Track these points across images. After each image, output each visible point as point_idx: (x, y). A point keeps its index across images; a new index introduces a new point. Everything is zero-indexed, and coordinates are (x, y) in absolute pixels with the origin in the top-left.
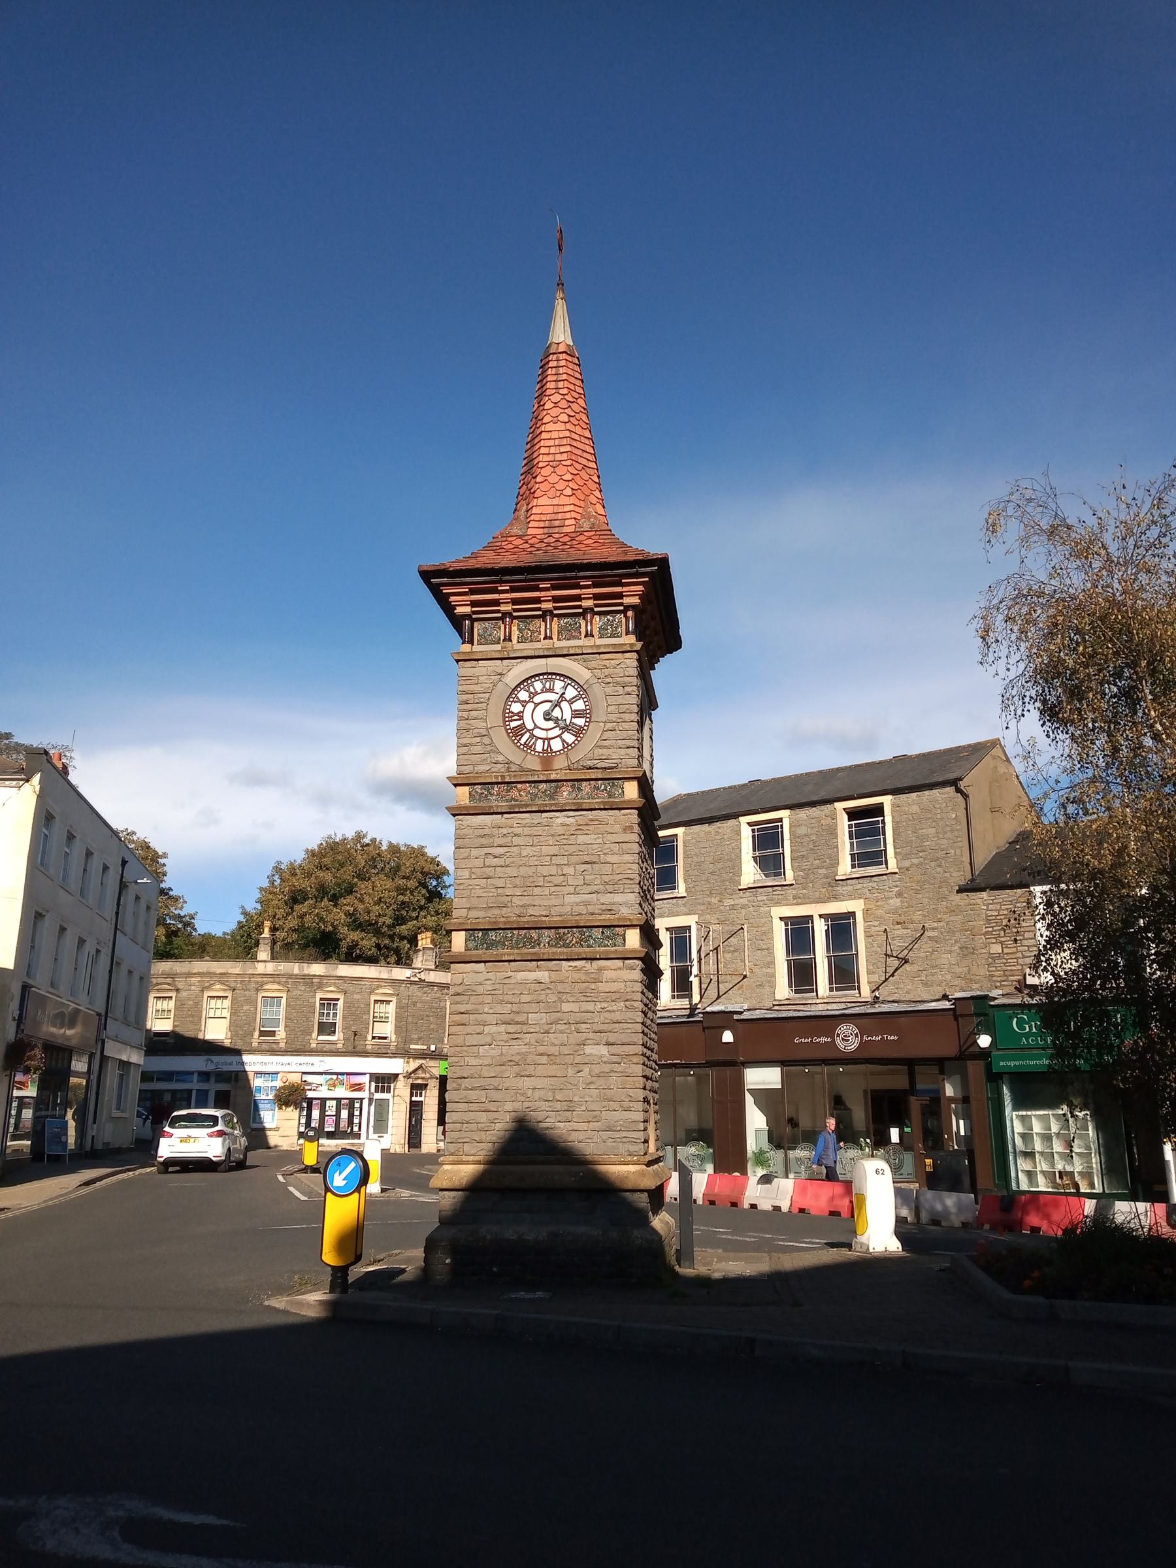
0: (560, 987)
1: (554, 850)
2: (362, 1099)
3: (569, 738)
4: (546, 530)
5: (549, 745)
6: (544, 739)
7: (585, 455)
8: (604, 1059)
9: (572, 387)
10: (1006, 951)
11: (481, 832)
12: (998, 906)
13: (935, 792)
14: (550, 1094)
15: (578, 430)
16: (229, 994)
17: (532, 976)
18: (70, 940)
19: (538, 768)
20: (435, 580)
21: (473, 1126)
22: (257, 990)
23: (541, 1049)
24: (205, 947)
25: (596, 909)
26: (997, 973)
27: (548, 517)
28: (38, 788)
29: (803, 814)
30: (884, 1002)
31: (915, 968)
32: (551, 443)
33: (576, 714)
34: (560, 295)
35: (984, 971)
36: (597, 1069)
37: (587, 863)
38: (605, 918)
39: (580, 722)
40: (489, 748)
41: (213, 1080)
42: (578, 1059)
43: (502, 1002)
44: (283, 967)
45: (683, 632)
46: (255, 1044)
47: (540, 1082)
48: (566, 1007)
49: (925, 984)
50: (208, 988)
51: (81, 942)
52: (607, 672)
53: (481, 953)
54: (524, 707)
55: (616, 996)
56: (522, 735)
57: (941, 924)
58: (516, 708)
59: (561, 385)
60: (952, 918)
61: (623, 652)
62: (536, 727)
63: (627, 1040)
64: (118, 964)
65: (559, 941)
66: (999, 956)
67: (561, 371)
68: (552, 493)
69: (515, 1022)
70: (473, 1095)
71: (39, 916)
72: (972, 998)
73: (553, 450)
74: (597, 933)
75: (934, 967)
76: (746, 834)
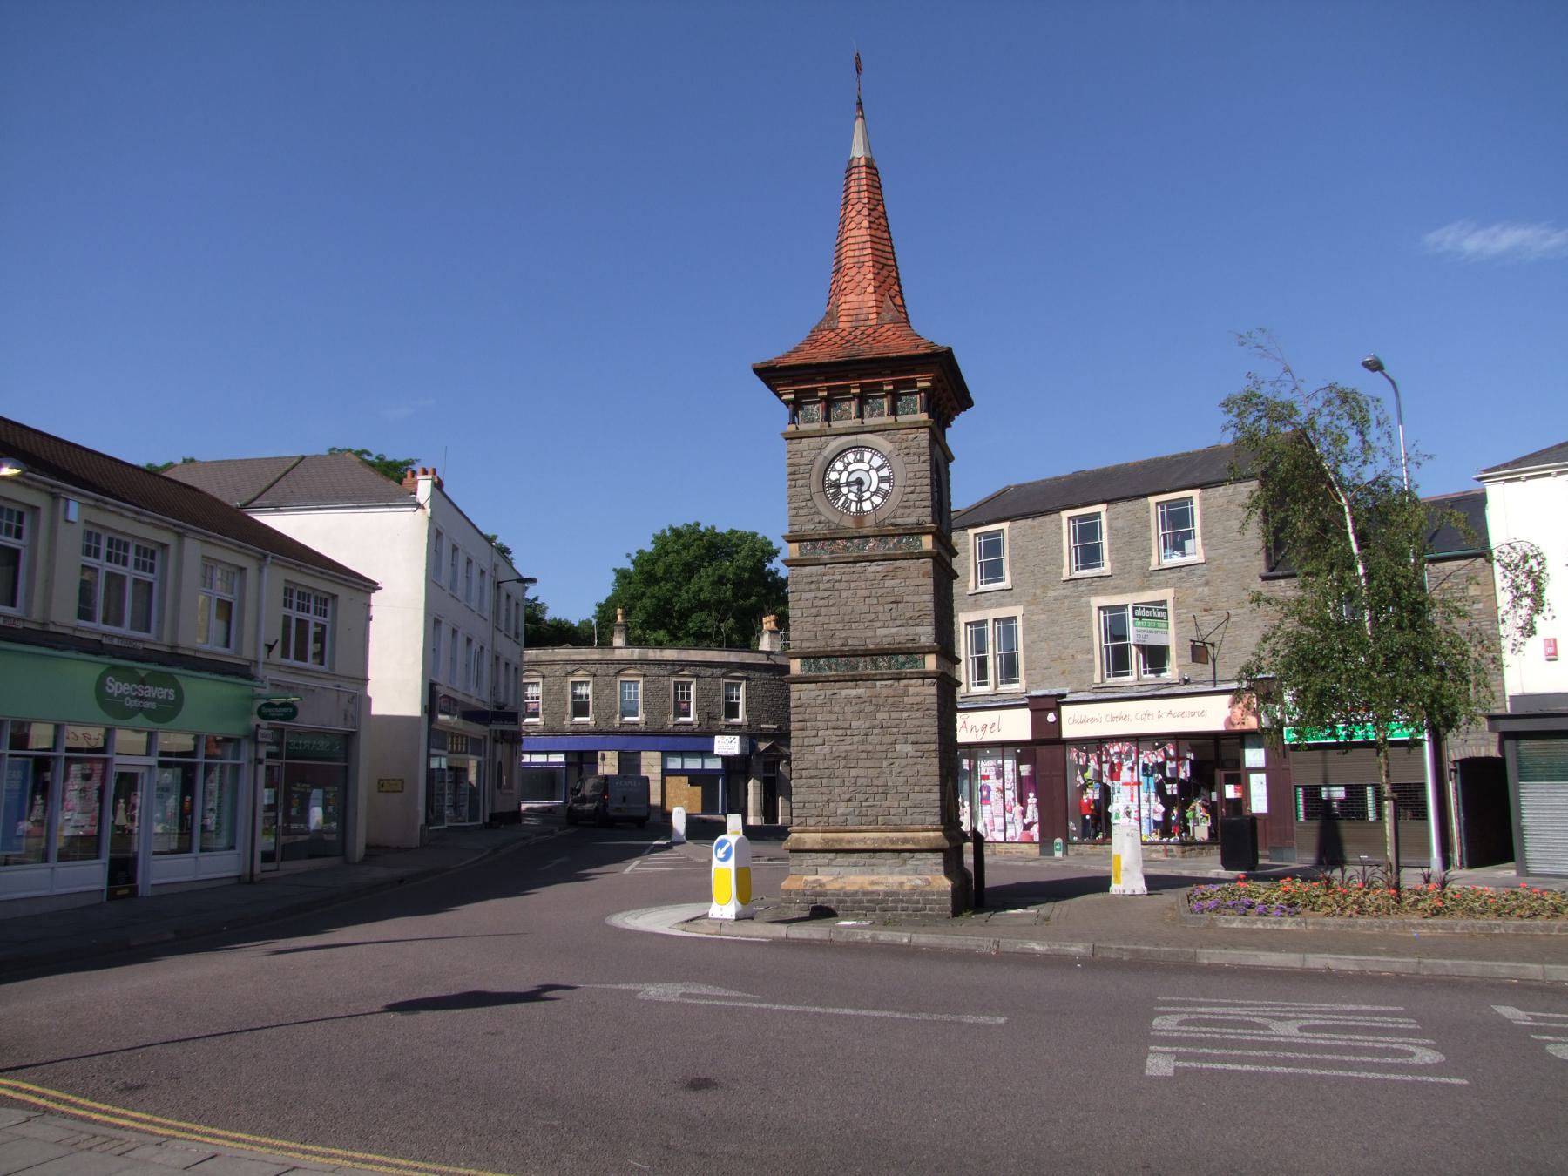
1: (867, 593)
17: (854, 692)
20: (770, 375)
24: (562, 635)
25: (902, 639)
29: (1121, 507)
33: (882, 480)
34: (859, 123)
36: (903, 762)
44: (636, 653)
45: (972, 395)
48: (879, 716)
50: (572, 674)
55: (917, 706)
69: (845, 732)
71: (437, 622)
76: (1065, 521)
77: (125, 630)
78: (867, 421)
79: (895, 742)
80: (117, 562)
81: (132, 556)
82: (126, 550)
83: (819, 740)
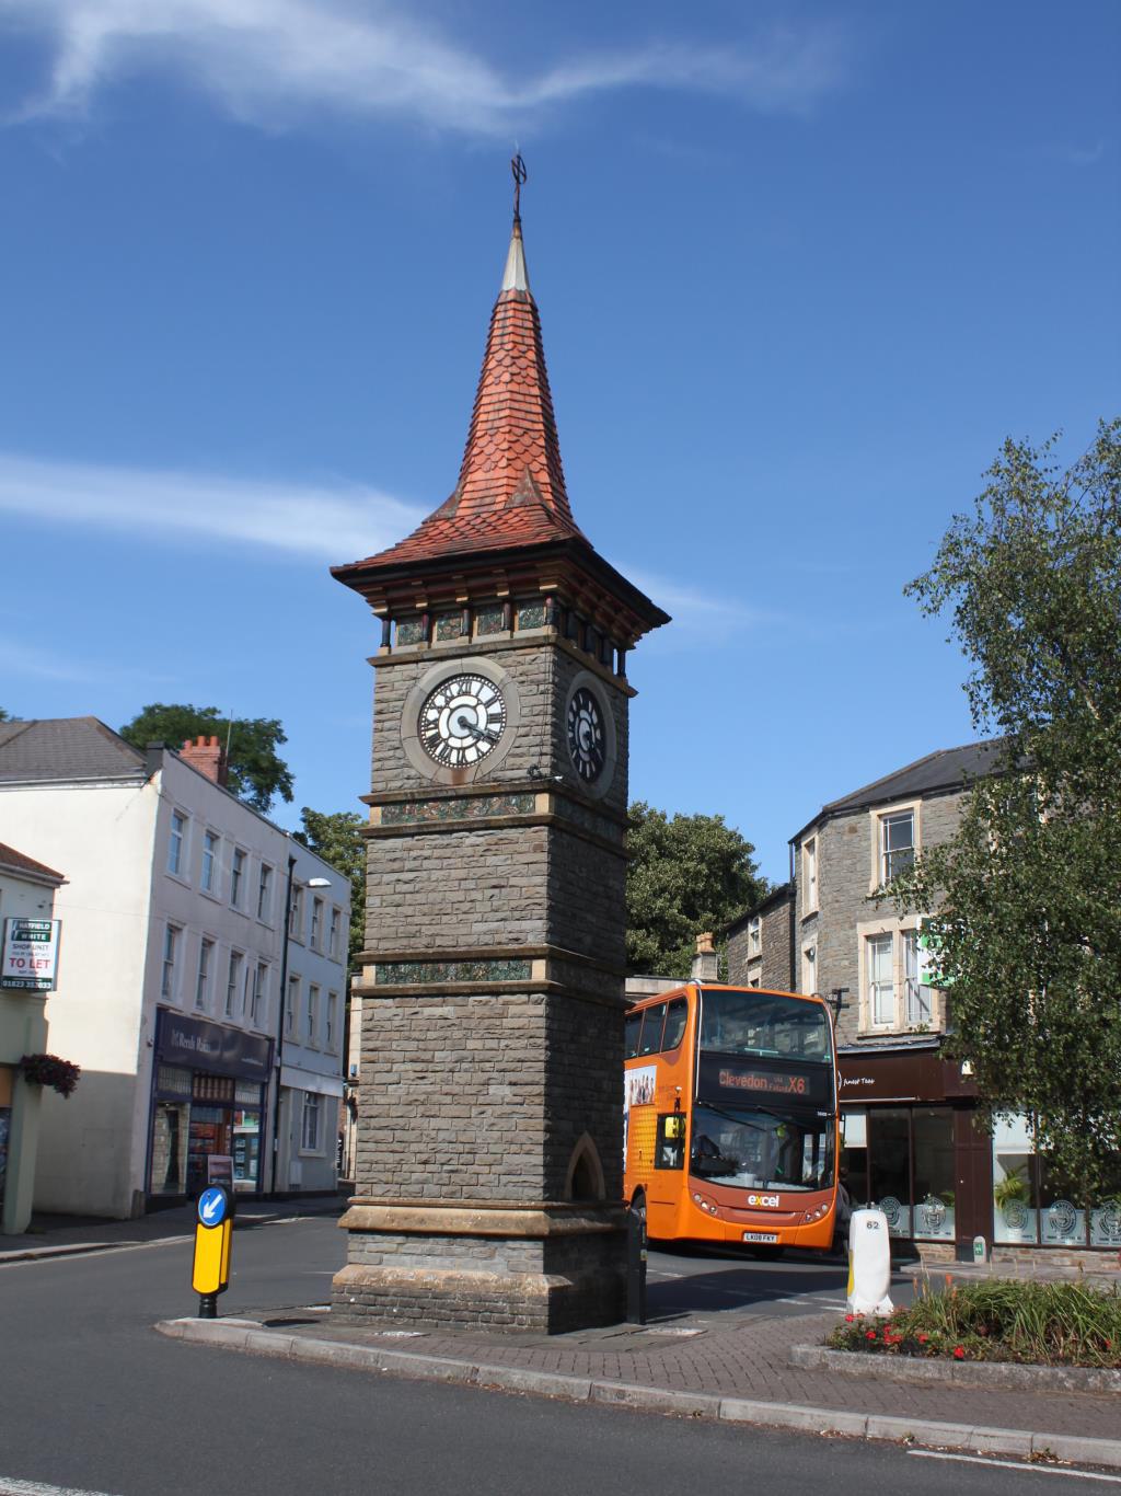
0: (465, 1023)
1: (462, 873)
3: (484, 746)
4: (476, 510)
5: (464, 756)
6: (458, 749)
8: (506, 1100)
9: (519, 339)
11: (393, 856)
14: (454, 1135)
15: (523, 389)
17: (438, 1011)
18: (218, 958)
19: (449, 782)
21: (381, 1167)
23: (446, 1089)
25: (503, 938)
27: (480, 494)
28: (159, 787)
32: (490, 408)
33: (492, 719)
36: (498, 1110)
37: (494, 887)
39: (495, 727)
40: (402, 762)
42: (481, 1099)
43: (408, 1039)
48: (471, 1044)
51: (236, 956)
52: (521, 669)
54: (440, 713)
55: (519, 1032)
56: (437, 746)
58: (432, 715)
59: (506, 339)
61: (514, 649)
62: (451, 735)
64: (293, 980)
67: (508, 322)
68: (486, 467)
70: (381, 1134)
71: (173, 930)
73: (491, 416)
74: (503, 965)
79: (486, 1084)
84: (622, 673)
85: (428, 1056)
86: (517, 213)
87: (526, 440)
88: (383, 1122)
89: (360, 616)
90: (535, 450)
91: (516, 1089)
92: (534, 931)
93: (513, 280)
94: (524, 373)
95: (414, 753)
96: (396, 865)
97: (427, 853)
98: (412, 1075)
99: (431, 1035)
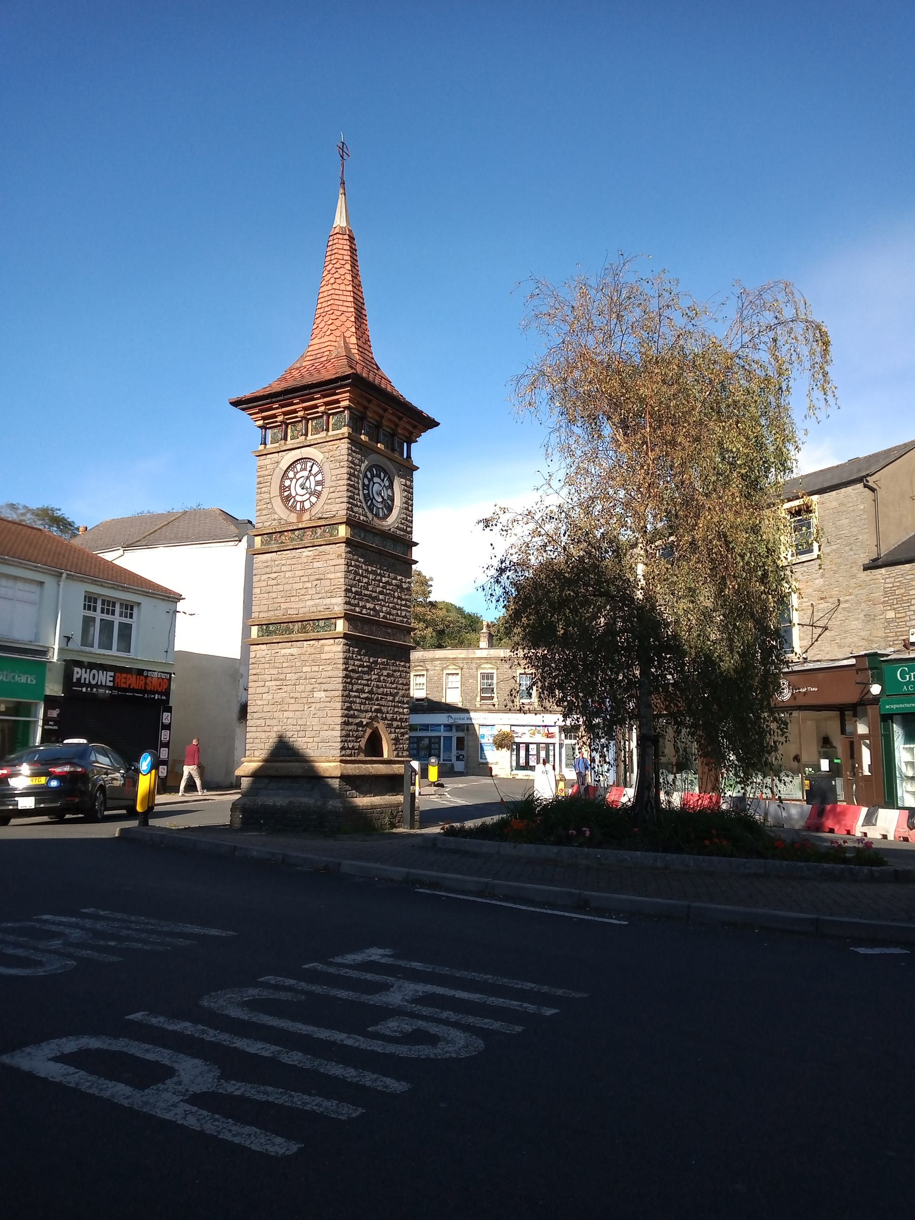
2: (554, 744)
3: (313, 499)
7: (345, 304)
10: (898, 616)
12: (892, 580)
13: (849, 489)
16: (459, 671)
17: (288, 651)
22: (477, 669)
25: (321, 608)
26: (890, 635)
30: (811, 662)
31: (833, 633)
33: (318, 483)
35: (881, 633)
37: (317, 580)
38: (327, 614)
39: (319, 488)
41: (454, 730)
45: (420, 408)
46: (478, 706)
47: (291, 714)
48: (305, 669)
49: (840, 646)
53: (266, 639)
57: (851, 597)
58: (287, 483)
59: (333, 257)
60: (861, 592)
63: (333, 688)
65: (303, 630)
66: (893, 620)
68: (319, 336)
69: (281, 680)
72: (866, 655)
75: (845, 632)
77: (114, 652)
78: (310, 437)
79: (312, 691)
80: (108, 613)
81: (99, 606)
82: (95, 602)
83: (265, 690)
84: (409, 456)
85: (283, 677)
86: (342, 179)
87: (343, 318)
88: (260, 715)
89: (248, 424)
90: (349, 324)
91: (328, 694)
92: (338, 604)
93: (340, 221)
94: (343, 277)
95: (278, 504)
96: (267, 570)
97: (284, 562)
98: (275, 688)
99: (285, 665)
